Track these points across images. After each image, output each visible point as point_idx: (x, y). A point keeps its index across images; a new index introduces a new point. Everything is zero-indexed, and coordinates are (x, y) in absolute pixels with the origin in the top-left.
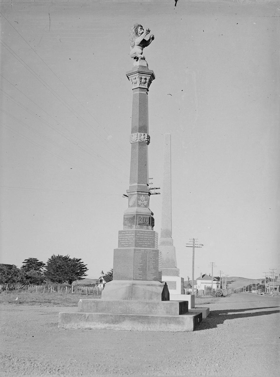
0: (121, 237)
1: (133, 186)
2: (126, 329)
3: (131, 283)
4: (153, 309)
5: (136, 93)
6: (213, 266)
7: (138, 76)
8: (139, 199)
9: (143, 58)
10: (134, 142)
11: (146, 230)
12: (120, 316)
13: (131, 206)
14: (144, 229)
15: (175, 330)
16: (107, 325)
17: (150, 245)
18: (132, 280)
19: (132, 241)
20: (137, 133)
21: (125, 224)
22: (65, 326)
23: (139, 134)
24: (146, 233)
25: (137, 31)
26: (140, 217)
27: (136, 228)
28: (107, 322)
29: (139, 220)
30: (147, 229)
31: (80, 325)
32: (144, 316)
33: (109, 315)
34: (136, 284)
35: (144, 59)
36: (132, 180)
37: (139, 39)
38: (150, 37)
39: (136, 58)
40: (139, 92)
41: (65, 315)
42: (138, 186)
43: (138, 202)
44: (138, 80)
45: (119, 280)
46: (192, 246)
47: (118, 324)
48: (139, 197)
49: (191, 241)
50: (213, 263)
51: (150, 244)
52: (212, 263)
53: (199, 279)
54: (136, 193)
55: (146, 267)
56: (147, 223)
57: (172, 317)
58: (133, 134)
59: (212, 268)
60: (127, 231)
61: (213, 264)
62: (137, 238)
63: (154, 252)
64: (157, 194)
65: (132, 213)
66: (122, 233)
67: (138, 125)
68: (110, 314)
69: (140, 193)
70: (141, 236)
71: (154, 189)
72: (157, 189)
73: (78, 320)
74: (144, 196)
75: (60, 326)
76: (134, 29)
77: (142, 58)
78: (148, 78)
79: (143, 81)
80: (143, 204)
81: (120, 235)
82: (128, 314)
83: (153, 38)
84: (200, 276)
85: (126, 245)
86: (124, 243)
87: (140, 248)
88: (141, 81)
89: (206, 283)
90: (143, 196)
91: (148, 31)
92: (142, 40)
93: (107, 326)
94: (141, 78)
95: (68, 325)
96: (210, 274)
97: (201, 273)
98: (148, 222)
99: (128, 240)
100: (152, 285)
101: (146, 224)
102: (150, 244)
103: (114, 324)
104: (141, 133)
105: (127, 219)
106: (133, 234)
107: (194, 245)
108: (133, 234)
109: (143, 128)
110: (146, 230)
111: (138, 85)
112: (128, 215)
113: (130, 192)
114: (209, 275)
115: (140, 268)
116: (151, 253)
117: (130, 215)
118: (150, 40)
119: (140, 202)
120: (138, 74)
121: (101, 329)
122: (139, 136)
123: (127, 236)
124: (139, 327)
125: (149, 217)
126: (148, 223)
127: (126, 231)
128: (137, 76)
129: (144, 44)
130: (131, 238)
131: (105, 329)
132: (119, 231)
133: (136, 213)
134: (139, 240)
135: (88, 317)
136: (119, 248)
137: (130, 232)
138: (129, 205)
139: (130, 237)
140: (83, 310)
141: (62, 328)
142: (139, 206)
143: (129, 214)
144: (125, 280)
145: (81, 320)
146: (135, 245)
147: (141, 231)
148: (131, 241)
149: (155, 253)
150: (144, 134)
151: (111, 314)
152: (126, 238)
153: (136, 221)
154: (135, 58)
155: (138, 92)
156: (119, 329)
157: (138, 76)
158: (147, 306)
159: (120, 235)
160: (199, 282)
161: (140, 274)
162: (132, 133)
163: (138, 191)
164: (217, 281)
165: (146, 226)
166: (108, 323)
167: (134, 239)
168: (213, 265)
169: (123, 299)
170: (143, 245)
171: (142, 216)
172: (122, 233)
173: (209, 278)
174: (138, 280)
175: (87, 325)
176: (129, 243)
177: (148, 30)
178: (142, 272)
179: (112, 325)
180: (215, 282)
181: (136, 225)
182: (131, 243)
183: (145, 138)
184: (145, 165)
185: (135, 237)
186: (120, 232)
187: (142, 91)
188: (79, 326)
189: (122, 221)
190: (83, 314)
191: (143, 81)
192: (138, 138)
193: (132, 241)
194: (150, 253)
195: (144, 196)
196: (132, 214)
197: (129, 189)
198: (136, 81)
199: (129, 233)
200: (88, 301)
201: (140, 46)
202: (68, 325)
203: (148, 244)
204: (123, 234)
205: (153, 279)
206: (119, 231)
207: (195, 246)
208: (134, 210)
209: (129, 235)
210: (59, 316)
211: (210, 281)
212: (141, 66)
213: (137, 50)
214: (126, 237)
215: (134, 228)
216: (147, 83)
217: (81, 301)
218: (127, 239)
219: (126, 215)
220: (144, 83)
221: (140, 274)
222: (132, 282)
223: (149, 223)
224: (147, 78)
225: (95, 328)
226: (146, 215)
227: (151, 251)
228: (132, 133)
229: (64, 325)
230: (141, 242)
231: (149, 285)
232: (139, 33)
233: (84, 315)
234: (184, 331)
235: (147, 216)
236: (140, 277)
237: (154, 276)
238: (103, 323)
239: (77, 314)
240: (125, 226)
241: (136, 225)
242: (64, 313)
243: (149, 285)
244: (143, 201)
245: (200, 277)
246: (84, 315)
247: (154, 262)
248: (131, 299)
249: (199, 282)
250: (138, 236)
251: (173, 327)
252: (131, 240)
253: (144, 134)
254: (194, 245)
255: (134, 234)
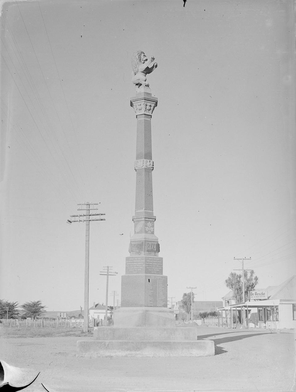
0: (129, 264)
1: (139, 212)
2: (148, 356)
3: (145, 310)
4: (172, 335)
5: (140, 119)
6: (115, 295)
7: (144, 102)
8: (146, 226)
9: (148, 85)
10: (140, 168)
11: (154, 257)
12: (142, 342)
13: (138, 233)
14: (152, 255)
15: (197, 355)
16: (128, 352)
17: (158, 271)
18: (143, 307)
19: (142, 267)
20: (143, 160)
21: (131, 251)
22: (84, 355)
23: (145, 160)
24: (155, 259)
25: (141, 58)
26: (148, 244)
27: (145, 255)
28: (128, 349)
29: (147, 247)
30: (155, 255)
31: (99, 354)
32: (166, 342)
33: (130, 342)
34: (149, 310)
35: (147, 86)
36: (137, 207)
37: (144, 67)
38: (154, 65)
39: (139, 85)
40: (144, 119)
41: (83, 343)
42: (145, 212)
43: (145, 229)
44: (143, 106)
45: (129, 307)
46: (107, 274)
47: (139, 351)
48: (146, 224)
49: (105, 269)
50: (114, 291)
51: (159, 270)
52: (114, 292)
53: (92, 308)
54: (144, 219)
55: (157, 293)
56: (155, 250)
57: (194, 342)
58: (138, 160)
59: (114, 297)
60: (136, 257)
61: (114, 293)
62: (147, 265)
63: (164, 279)
64: (102, 220)
65: (139, 239)
66: (130, 259)
67: (144, 151)
68: (130, 341)
69: (147, 219)
70: (151, 262)
71: (99, 215)
72: (102, 215)
73: (97, 348)
74: (151, 223)
75: (79, 355)
76: (138, 55)
77: (147, 85)
78: (153, 105)
79: (148, 107)
80: (150, 231)
81: (127, 261)
82: (149, 341)
83: (156, 66)
84: (93, 306)
85: (135, 271)
86: (133, 269)
87: (149, 275)
88: (146, 108)
89: (99, 313)
90: (149, 222)
91: (153, 59)
92: (147, 67)
93: (128, 353)
94: (146, 105)
95: (87, 354)
96: (103, 303)
97: (94, 303)
98: (156, 248)
99: (138, 267)
100: (163, 311)
101: (154, 250)
102: (159, 270)
103: (135, 351)
104: (146, 160)
105: (135, 245)
106: (143, 261)
107: (108, 273)
108: (143, 261)
109: (148, 156)
110: (154, 257)
111: (143, 112)
112: (135, 241)
113: (137, 218)
114: (103, 305)
115: (151, 294)
116: (161, 280)
117: (138, 241)
118: (153, 67)
119: (147, 229)
120: (144, 100)
121: (122, 356)
122: (145, 163)
123: (136, 262)
124: (161, 353)
125: (156, 243)
126: (156, 249)
127: (135, 257)
128: (143, 102)
129: (148, 71)
130: (140, 265)
131: (126, 356)
132: (127, 258)
133: (144, 240)
134: (148, 267)
135: (108, 345)
136: (127, 275)
137: (139, 259)
138: (135, 232)
139: (139, 263)
140: (99, 339)
141: (81, 357)
142: (146, 232)
143: (136, 240)
144: (135, 307)
145: (101, 348)
146: (145, 272)
147: (151, 257)
148: (140, 268)
149: (164, 280)
150: (150, 161)
151: (132, 341)
152: (135, 265)
153: (145, 248)
154: (137, 84)
155: (142, 118)
156: (141, 356)
157: (144, 102)
158: (166, 332)
159: (127, 261)
160: (91, 312)
161: (150, 301)
162: (136, 159)
163: (145, 218)
164: (110, 310)
165: (154, 253)
166: (129, 351)
167: (144, 265)
168: (115, 293)
169: (137, 326)
170: (152, 271)
171: (150, 243)
172: (130, 259)
173: (102, 307)
174: (149, 306)
175: (107, 353)
176: (139, 270)
177: (153, 58)
178: (152, 298)
179: (133, 352)
180: (109, 311)
181: (145, 252)
182: (140, 270)
183: (151, 165)
184: (151, 192)
185: (145, 263)
186: (127, 259)
187: (147, 117)
188: (98, 354)
189: (127, 247)
190: (102, 342)
191: (148, 107)
192: (145, 165)
193: (142, 267)
194: (159, 280)
195: (151, 223)
196: (140, 241)
197: (134, 215)
198: (141, 107)
199: (138, 260)
200: (104, 328)
201: (144, 73)
202: (87, 354)
203: (157, 270)
204: (131, 260)
205: (162, 305)
206: (127, 258)
207: (109, 274)
208: (141, 237)
209: (138, 261)
210: (77, 345)
211: (104, 311)
212: (146, 93)
213: (141, 77)
214: (135, 264)
215: (143, 255)
216: (151, 110)
217: (97, 329)
218: (135, 266)
219: (133, 241)
220: (149, 110)
221: (150, 301)
222: (144, 308)
223: (156, 249)
224: (152, 105)
225: (115, 355)
226: (154, 241)
227: (161, 277)
228: (136, 159)
229: (82, 355)
230: (151, 269)
231: (160, 311)
232: (142, 60)
233: (104, 343)
234: (206, 355)
235: (154, 243)
236: (151, 304)
237: (163, 303)
238: (124, 351)
239: (97, 342)
240: (131, 253)
241: (145, 252)
242: (82, 342)
243: (160, 311)
244: (149, 227)
245: (93, 307)
246: (104, 343)
247: (163, 289)
248: (144, 326)
249: (91, 312)
250: (147, 262)
251: (195, 352)
252: (141, 267)
253: (150, 161)
254: (108, 273)
255: (144, 261)
